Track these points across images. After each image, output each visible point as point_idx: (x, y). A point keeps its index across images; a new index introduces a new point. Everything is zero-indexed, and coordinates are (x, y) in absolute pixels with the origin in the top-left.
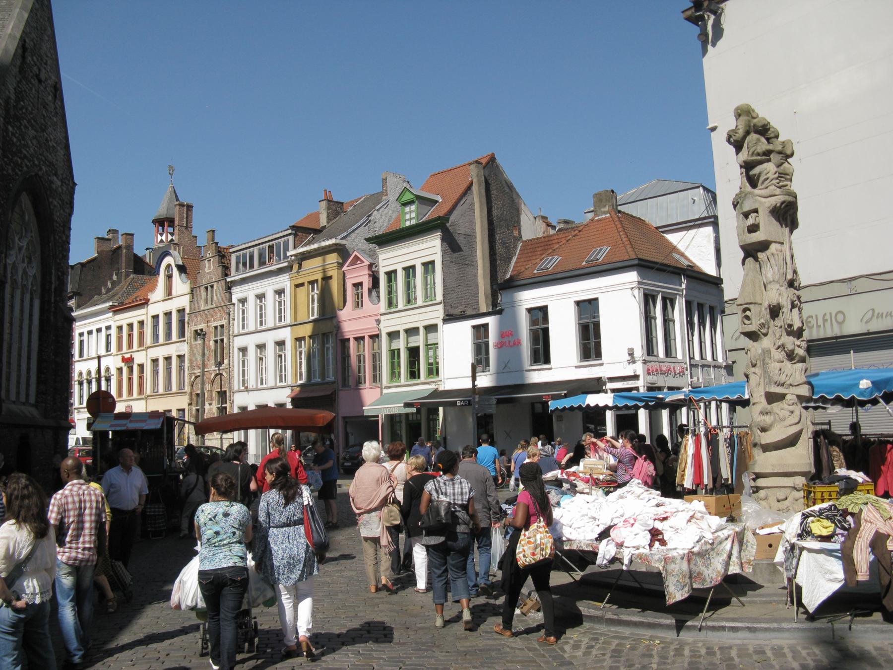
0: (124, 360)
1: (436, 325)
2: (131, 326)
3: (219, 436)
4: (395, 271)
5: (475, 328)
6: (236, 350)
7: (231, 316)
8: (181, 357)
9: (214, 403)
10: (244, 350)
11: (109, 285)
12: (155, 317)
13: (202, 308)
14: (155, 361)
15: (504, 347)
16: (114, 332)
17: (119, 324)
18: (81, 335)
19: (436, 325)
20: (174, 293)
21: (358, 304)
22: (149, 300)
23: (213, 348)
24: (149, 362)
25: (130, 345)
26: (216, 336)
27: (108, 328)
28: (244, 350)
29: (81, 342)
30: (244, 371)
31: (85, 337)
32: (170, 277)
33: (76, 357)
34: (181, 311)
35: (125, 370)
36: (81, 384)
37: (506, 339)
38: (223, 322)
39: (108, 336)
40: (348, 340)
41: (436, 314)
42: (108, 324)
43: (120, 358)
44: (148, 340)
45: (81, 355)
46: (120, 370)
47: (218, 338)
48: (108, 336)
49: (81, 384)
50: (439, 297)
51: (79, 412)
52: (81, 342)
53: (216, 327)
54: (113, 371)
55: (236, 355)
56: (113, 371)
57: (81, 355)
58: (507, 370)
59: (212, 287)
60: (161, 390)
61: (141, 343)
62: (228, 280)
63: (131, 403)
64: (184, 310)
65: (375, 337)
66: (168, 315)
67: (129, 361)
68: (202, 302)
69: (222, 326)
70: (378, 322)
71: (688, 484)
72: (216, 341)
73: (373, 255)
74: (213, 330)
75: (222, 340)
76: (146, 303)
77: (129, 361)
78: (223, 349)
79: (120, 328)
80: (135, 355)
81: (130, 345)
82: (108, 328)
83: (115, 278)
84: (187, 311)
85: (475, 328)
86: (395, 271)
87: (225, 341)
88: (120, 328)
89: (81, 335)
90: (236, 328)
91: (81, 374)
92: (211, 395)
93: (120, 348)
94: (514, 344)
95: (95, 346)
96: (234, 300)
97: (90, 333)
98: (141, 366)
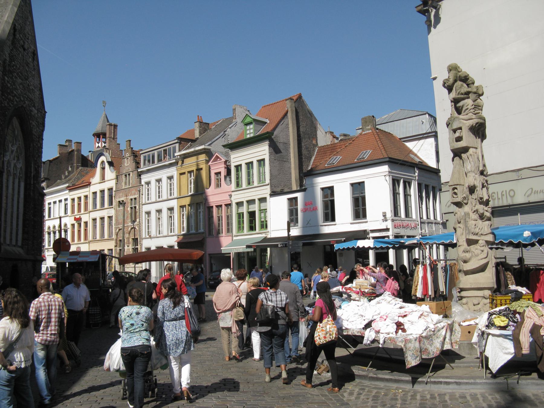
0: (76, 219)
1: (266, 198)
2: (80, 198)
4: (241, 165)
5: (290, 200)
6: (144, 213)
7: (141, 193)
8: (110, 218)
9: (130, 245)
10: (148, 213)
11: (67, 174)
12: (95, 193)
13: (123, 188)
14: (94, 220)
15: (307, 211)
16: (69, 202)
17: (72, 197)
18: (49, 204)
19: (266, 198)
20: (106, 179)
21: (218, 185)
22: (90, 183)
23: (129, 212)
24: (91, 220)
25: (79, 210)
26: (131, 204)
27: (66, 200)
28: (148, 213)
29: (50, 208)
30: (148, 226)
31: (52, 206)
32: (103, 168)
33: (47, 217)
34: (110, 190)
35: (76, 225)
36: (49, 234)
37: (308, 207)
38: (136, 196)
39: (66, 205)
40: (212, 207)
41: (266, 191)
42: (66, 197)
43: (73, 218)
44: (90, 207)
45: (49, 216)
46: (73, 225)
47: (133, 206)
48: (66, 205)
49: (49, 234)
50: (268, 181)
51: (48, 251)
52: (50, 208)
53: (131, 199)
54: (69, 226)
55: (144, 216)
56: (69, 226)
57: (49, 216)
58: (309, 225)
59: (129, 175)
60: (98, 237)
61: (86, 209)
62: (139, 170)
63: (80, 245)
64: (112, 189)
65: (228, 205)
66: (102, 192)
67: (78, 220)
68: (123, 184)
69: (135, 199)
70: (231, 196)
72: (132, 208)
73: (227, 155)
74: (129, 201)
75: (135, 207)
76: (89, 184)
77: (78, 220)
78: (136, 212)
79: (73, 200)
80: (82, 216)
81: (79, 210)
82: (66, 200)
83: (70, 169)
84: (114, 189)
85: (290, 200)
86: (241, 165)
87: (137, 208)
88: (73, 200)
89: (49, 204)
90: (144, 199)
91: (49, 228)
92: (129, 241)
93: (73, 212)
94: (313, 210)
95: (58, 210)
96: (143, 183)
97: (55, 203)
98: (86, 223)
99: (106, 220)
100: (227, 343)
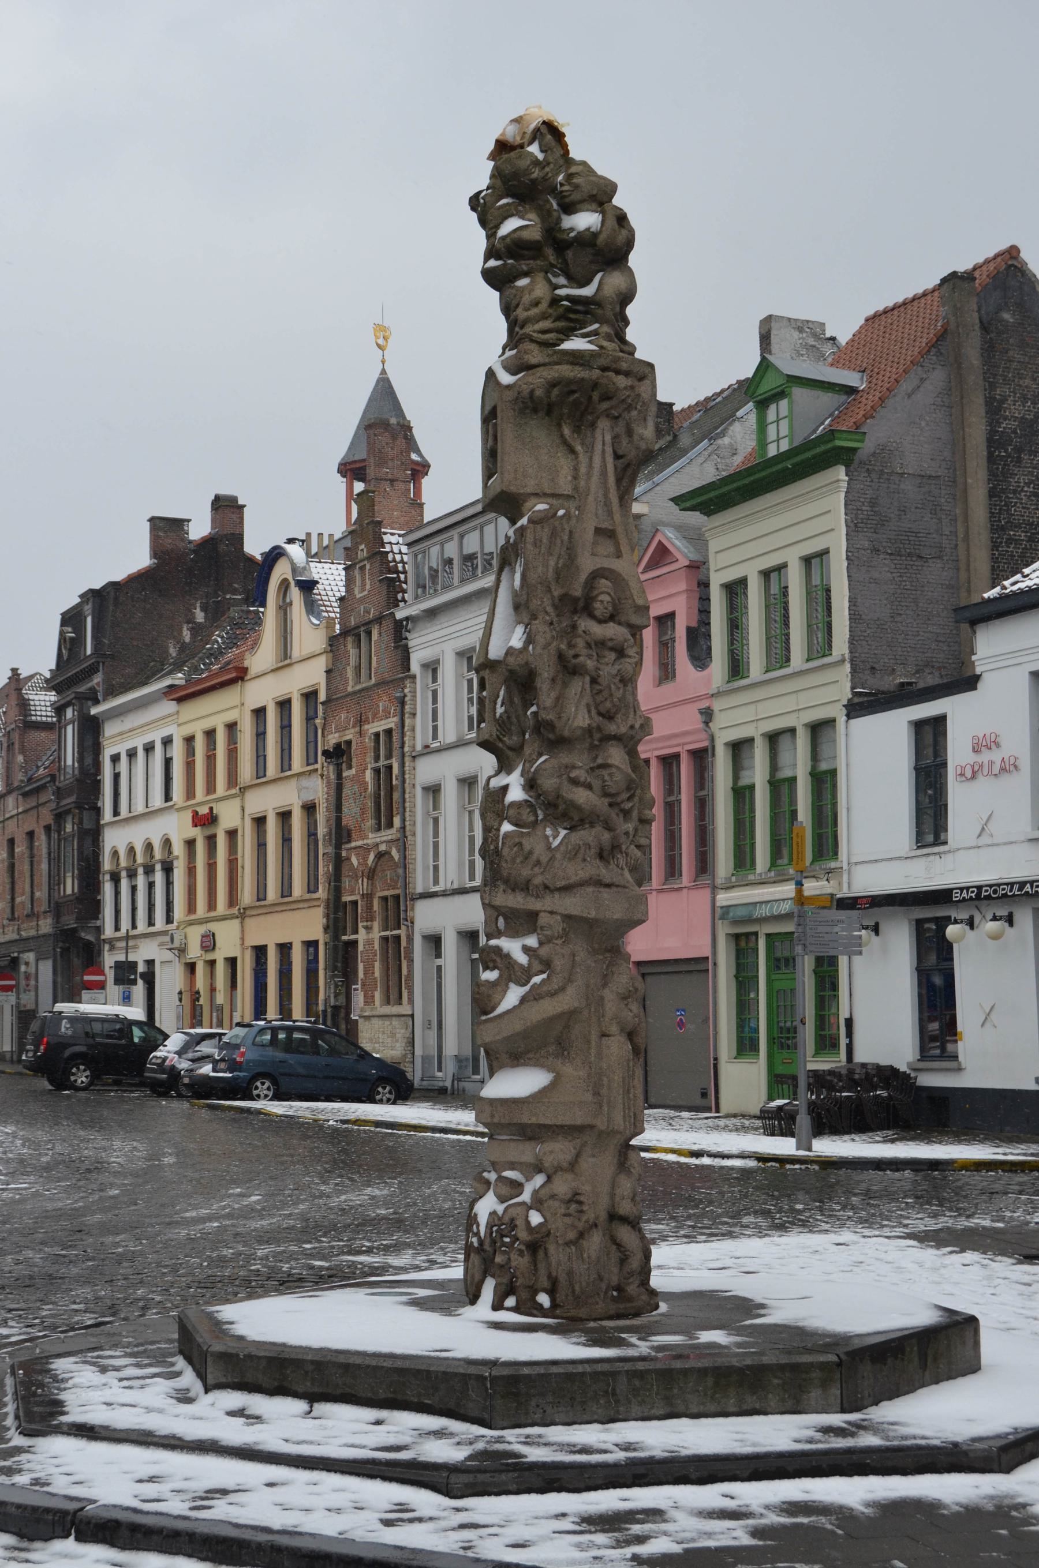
0: (198, 820)
1: (834, 720)
2: (210, 734)
3: (34, 923)
4: (743, 582)
5: (919, 726)
6: (419, 791)
7: (407, 708)
8: (310, 808)
9: (376, 925)
10: (434, 791)
11: (187, 635)
12: (260, 713)
13: (350, 689)
14: (260, 822)
15: (980, 778)
16: (177, 752)
17: (187, 730)
18: (115, 759)
19: (834, 720)
20: (296, 653)
21: (667, 672)
22: (245, 670)
23: (370, 788)
24: (248, 823)
25: (211, 788)
26: (377, 759)
27: (167, 742)
28: (434, 791)
29: (117, 777)
30: (436, 845)
31: (123, 766)
32: (284, 608)
33: (107, 816)
34: (310, 696)
35: (200, 847)
36: (116, 878)
37: (985, 757)
38: (391, 723)
39: (168, 762)
40: (647, 761)
41: (836, 688)
42: (165, 732)
43: (188, 815)
44: (246, 770)
45: (116, 812)
46: (190, 844)
47: (382, 762)
48: (168, 762)
49: (116, 878)
50: (841, 645)
51: (112, 948)
52: (117, 777)
53: (377, 735)
54: (178, 849)
55: (418, 802)
56: (178, 849)
57: (116, 812)
58: (985, 840)
59: (369, 633)
60: (272, 893)
61: (232, 779)
62: (400, 615)
63: (213, 927)
64: (315, 693)
65: (701, 757)
66: (284, 705)
67: (207, 821)
68: (350, 673)
69: (389, 732)
70: (708, 715)
71: (773, 977)
72: (377, 771)
73: (698, 539)
74: (369, 742)
75: (390, 768)
76: (240, 675)
77: (207, 821)
78: (391, 789)
79: (189, 740)
80: (220, 809)
81: (211, 788)
82: (167, 742)
83: (200, 616)
84: (322, 696)
85: (919, 726)
86: (743, 582)
87: (396, 770)
88: (189, 740)
89: (115, 759)
90: (419, 736)
91: (115, 854)
92: (369, 907)
93: (190, 793)
94: (1003, 770)
95: (141, 785)
96: (415, 667)
97: (132, 754)
98: (232, 834)
99: (272, 827)
100: (197, 1415)
